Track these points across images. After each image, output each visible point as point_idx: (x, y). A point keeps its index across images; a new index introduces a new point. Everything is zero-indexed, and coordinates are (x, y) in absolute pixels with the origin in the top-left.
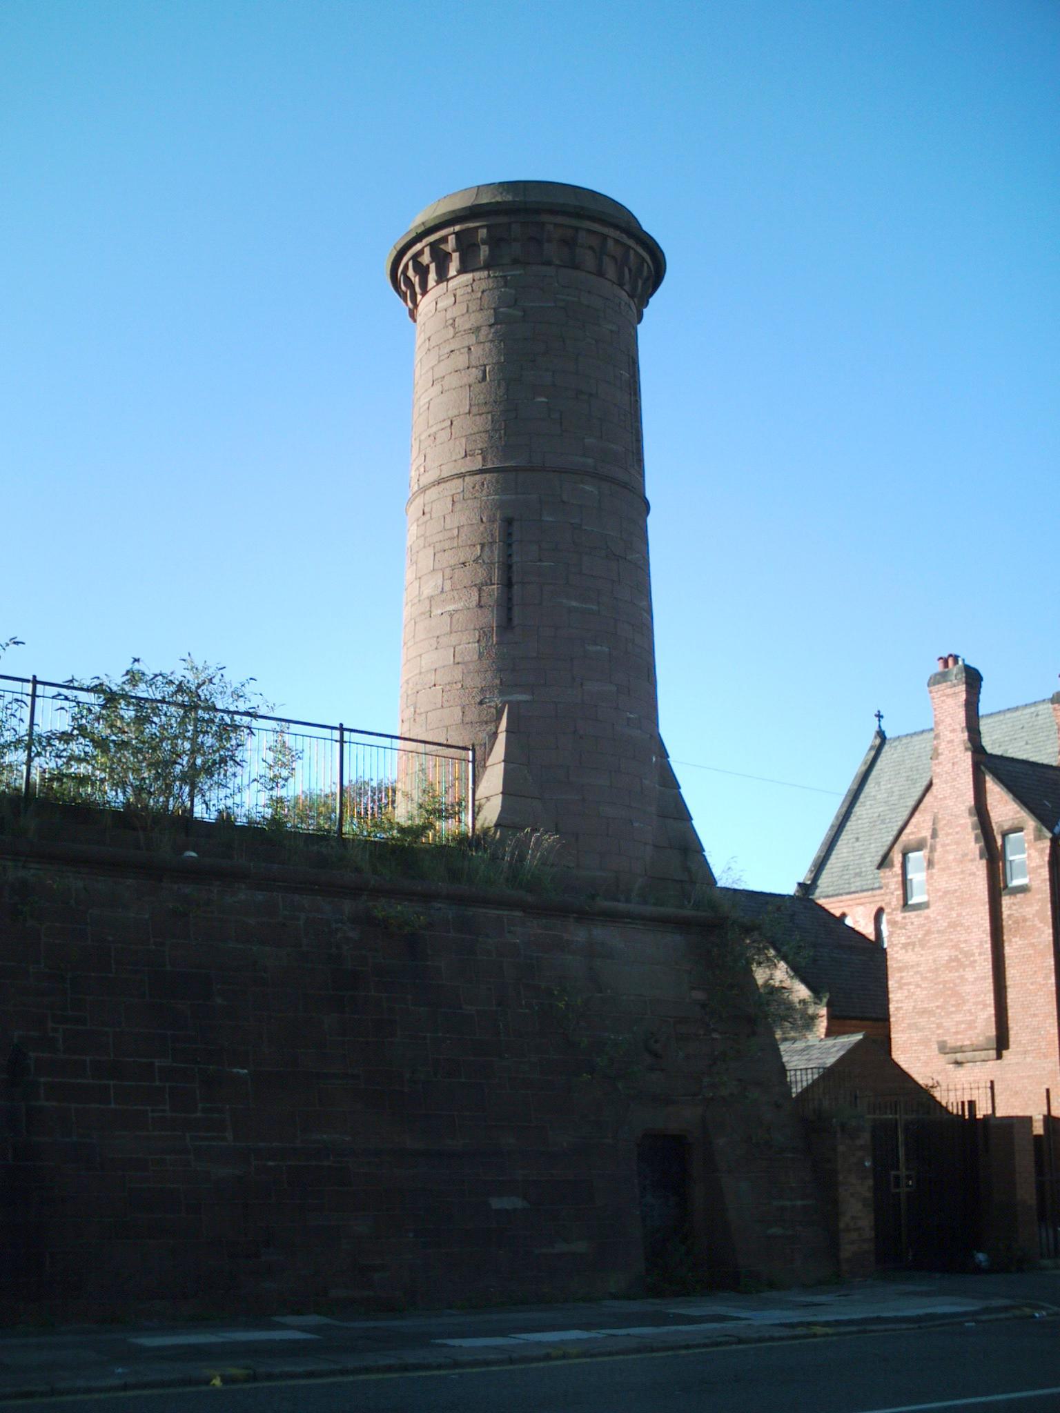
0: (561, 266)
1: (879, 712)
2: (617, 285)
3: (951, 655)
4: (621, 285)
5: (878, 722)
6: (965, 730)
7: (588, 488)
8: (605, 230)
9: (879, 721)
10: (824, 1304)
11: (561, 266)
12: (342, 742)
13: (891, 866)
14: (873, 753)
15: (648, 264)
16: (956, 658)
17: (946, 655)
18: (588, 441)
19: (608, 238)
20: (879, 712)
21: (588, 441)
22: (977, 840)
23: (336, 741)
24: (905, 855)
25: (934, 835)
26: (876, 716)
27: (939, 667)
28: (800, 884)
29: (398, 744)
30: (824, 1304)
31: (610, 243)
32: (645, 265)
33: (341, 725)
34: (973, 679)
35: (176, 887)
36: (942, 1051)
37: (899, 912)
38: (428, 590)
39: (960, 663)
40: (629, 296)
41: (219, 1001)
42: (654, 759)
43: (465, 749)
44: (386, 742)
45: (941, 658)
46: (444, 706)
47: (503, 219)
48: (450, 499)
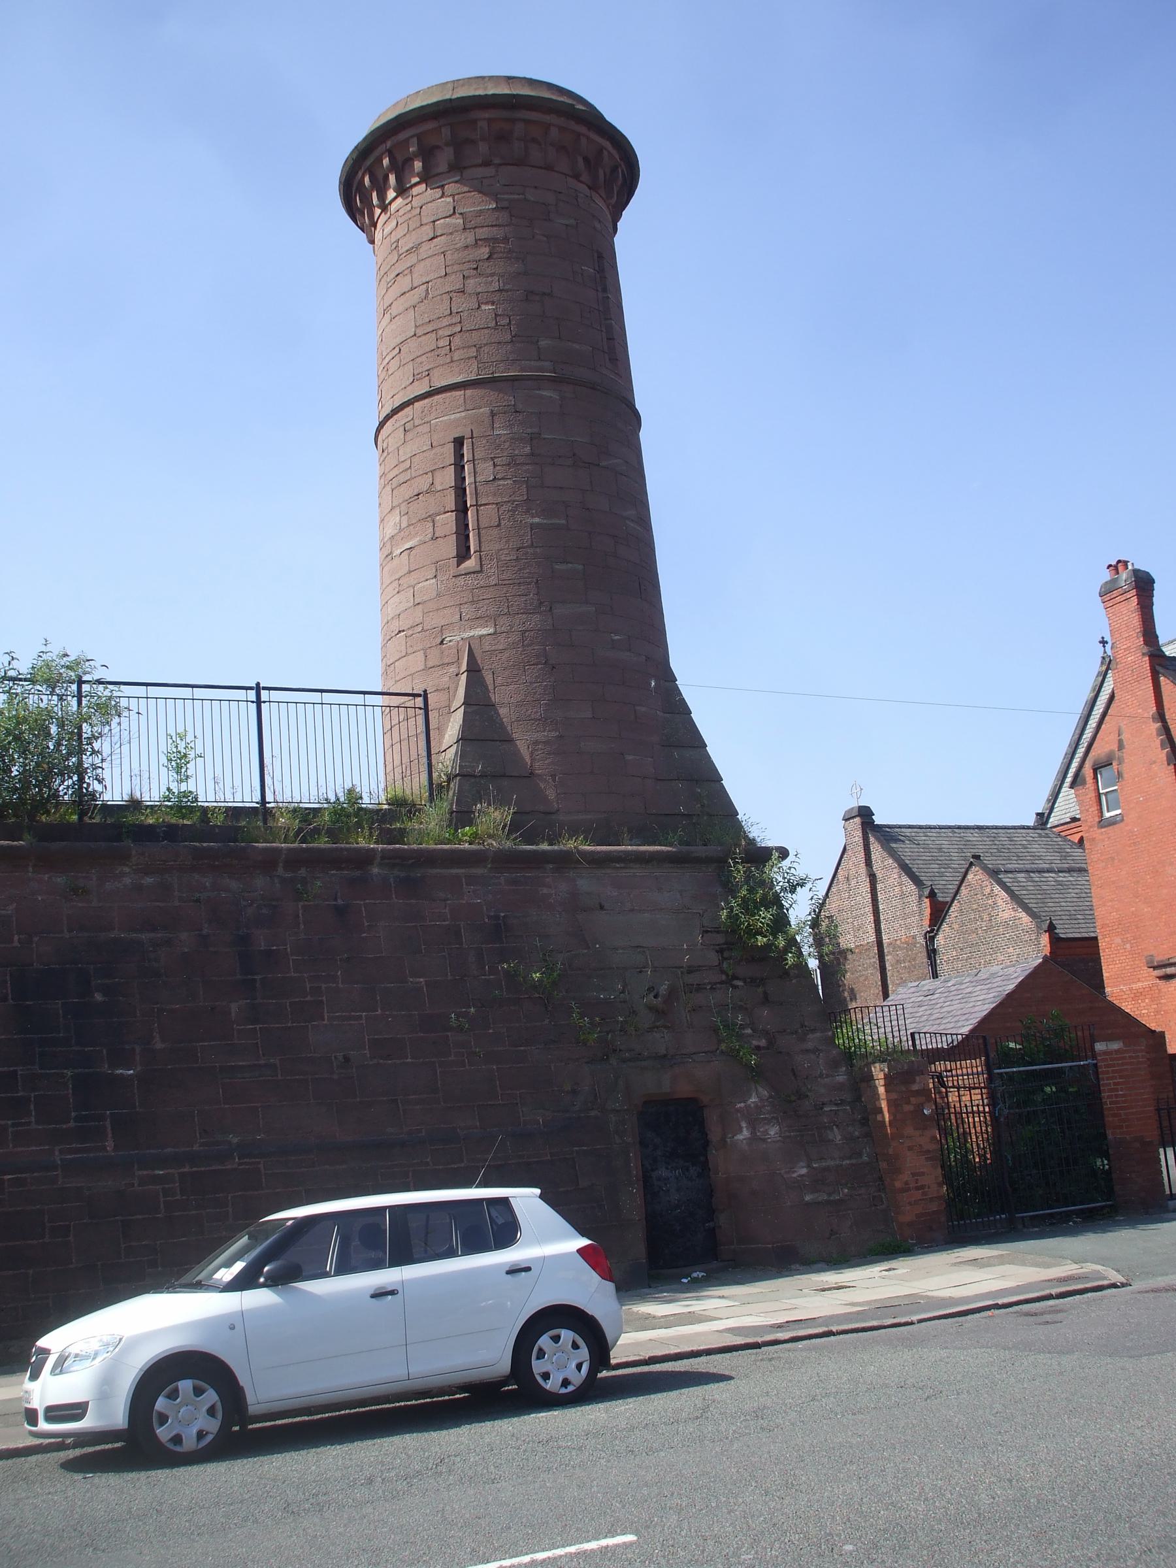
0: (501, 165)
1: (1103, 638)
2: (571, 177)
3: (1119, 562)
4: (577, 177)
5: (1103, 649)
6: (1140, 635)
7: (545, 393)
8: (548, 118)
9: (1104, 646)
10: (847, 1287)
11: (501, 165)
12: (259, 702)
13: (1084, 783)
14: (1100, 678)
15: (609, 152)
16: (1125, 563)
17: (1114, 563)
18: (543, 343)
19: (581, 137)
20: (1103, 638)
21: (543, 343)
22: (1163, 747)
23: (253, 702)
24: (1095, 771)
25: (1121, 746)
26: (1100, 642)
27: (1107, 576)
28: (1038, 814)
29: (379, 700)
30: (847, 1287)
31: (584, 141)
32: (605, 153)
33: (258, 684)
34: (1144, 585)
35: (46, 877)
36: (1150, 965)
37: (1095, 829)
38: (390, 531)
39: (1130, 567)
40: (590, 188)
41: (99, 997)
42: (653, 684)
43: (415, 695)
44: (316, 697)
45: (1110, 566)
46: (409, 652)
47: (430, 125)
48: (402, 429)
